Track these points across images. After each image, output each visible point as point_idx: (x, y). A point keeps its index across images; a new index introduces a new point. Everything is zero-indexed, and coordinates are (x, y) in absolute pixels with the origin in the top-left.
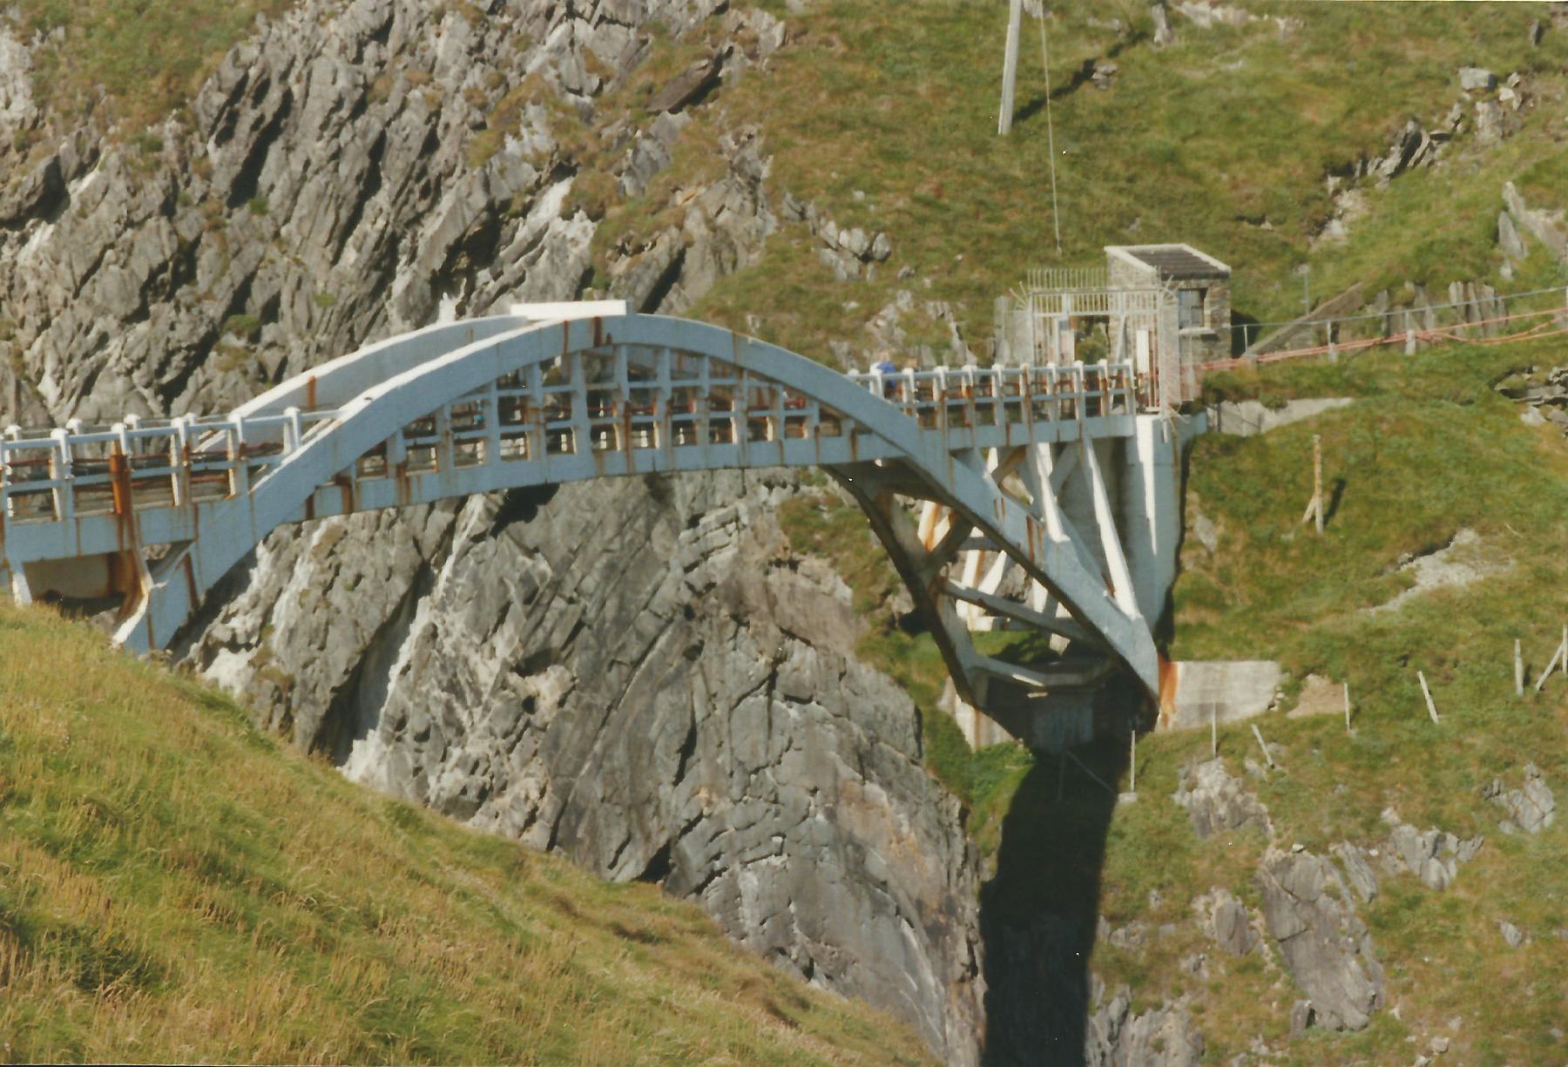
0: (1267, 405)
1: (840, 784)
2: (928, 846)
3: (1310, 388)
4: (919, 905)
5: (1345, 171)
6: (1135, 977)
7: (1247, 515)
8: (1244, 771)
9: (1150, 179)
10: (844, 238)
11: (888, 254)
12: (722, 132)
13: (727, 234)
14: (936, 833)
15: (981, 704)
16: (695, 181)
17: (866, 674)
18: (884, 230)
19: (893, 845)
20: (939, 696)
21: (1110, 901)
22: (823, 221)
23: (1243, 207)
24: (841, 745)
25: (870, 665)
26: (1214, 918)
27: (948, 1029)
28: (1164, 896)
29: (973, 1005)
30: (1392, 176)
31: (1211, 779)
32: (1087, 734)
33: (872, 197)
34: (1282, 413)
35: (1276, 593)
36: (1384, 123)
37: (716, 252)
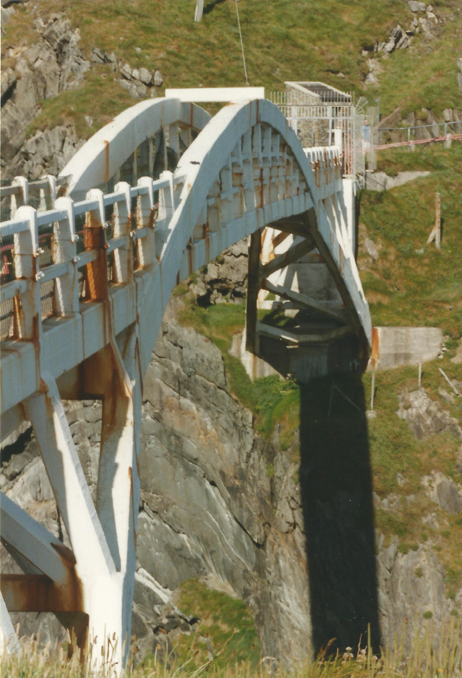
0: (389, 175)
1: (164, 398)
2: (225, 438)
3: (409, 165)
4: (222, 474)
5: (370, 48)
6: (402, 530)
7: (394, 239)
8: (441, 397)
9: (279, 48)
10: (136, 73)
11: (162, 83)
12: (35, 17)
13: (40, 72)
14: (232, 430)
15: (257, 351)
16: (21, 43)
17: (188, 334)
18: (158, 69)
19: (201, 437)
20: (230, 347)
21: (377, 482)
22: (120, 64)
23: (329, 64)
24: (165, 374)
25: (192, 329)
26: (435, 489)
27: (282, 563)
28: (405, 477)
29: (295, 547)
30: (390, 52)
31: (419, 402)
32: (324, 371)
33: (146, 51)
34: (396, 178)
35: (422, 287)
36: (386, 25)
37: (35, 82)
